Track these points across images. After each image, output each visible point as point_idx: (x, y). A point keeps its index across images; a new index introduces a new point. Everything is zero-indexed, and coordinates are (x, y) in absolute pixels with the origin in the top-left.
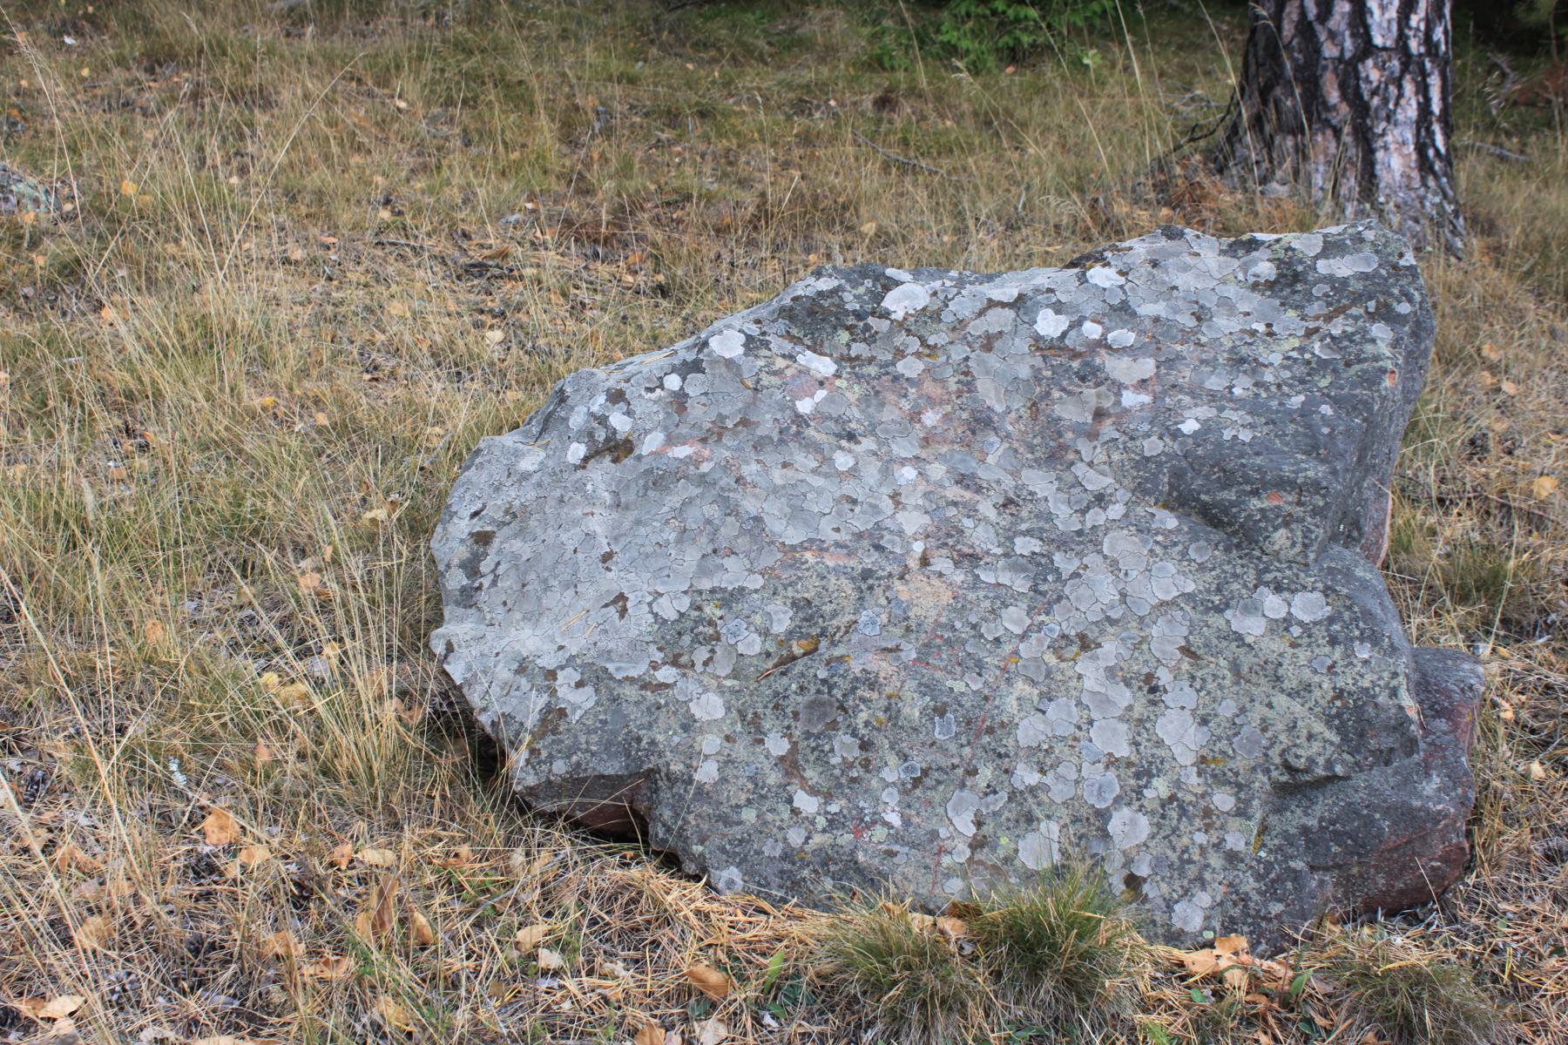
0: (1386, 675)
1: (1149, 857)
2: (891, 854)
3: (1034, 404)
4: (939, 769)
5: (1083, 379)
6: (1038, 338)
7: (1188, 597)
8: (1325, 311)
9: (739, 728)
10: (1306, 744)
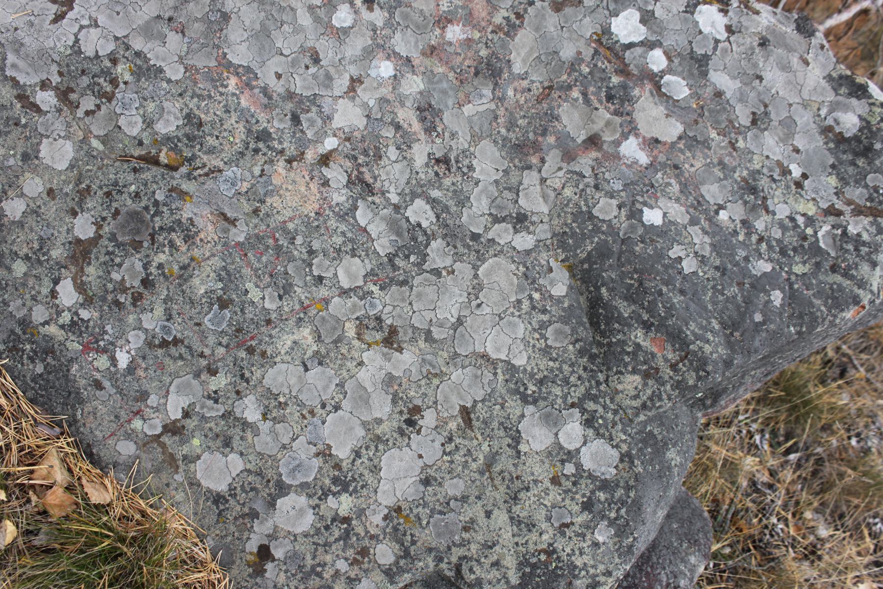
0: (601, 568)
1: (290, 547)
2: (98, 385)
3: (550, 88)
4: (189, 348)
5: (610, 98)
6: (606, 31)
7: (511, 368)
8: (862, 202)
9: (68, 189)
10: (487, 567)
